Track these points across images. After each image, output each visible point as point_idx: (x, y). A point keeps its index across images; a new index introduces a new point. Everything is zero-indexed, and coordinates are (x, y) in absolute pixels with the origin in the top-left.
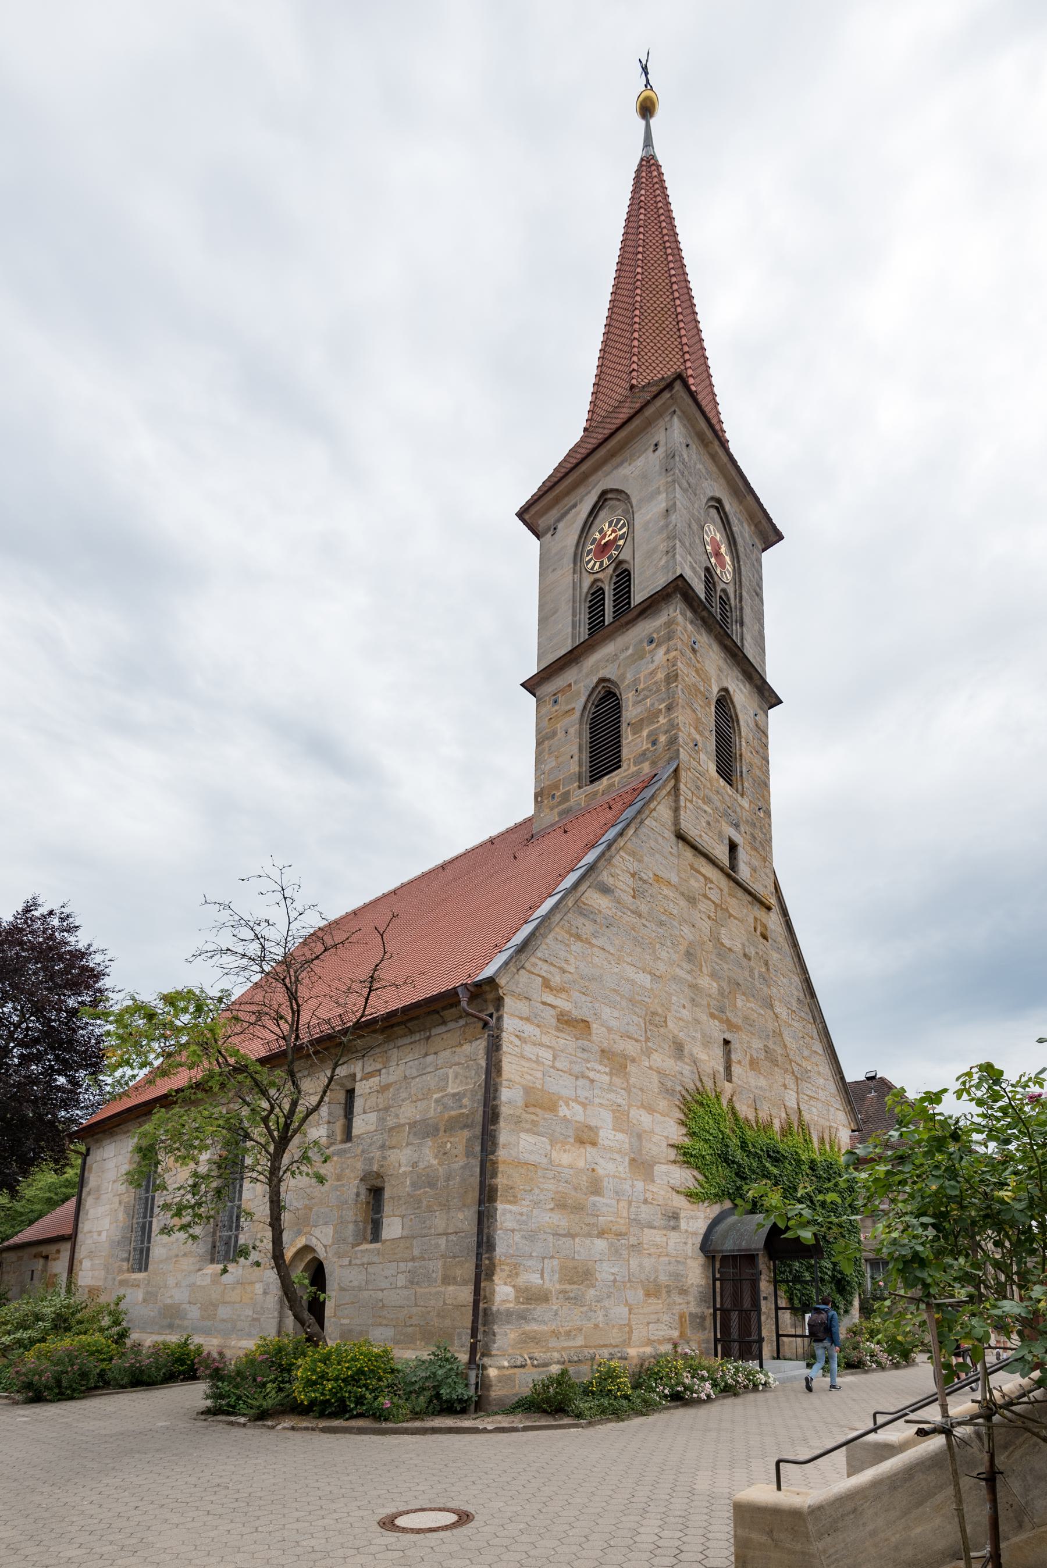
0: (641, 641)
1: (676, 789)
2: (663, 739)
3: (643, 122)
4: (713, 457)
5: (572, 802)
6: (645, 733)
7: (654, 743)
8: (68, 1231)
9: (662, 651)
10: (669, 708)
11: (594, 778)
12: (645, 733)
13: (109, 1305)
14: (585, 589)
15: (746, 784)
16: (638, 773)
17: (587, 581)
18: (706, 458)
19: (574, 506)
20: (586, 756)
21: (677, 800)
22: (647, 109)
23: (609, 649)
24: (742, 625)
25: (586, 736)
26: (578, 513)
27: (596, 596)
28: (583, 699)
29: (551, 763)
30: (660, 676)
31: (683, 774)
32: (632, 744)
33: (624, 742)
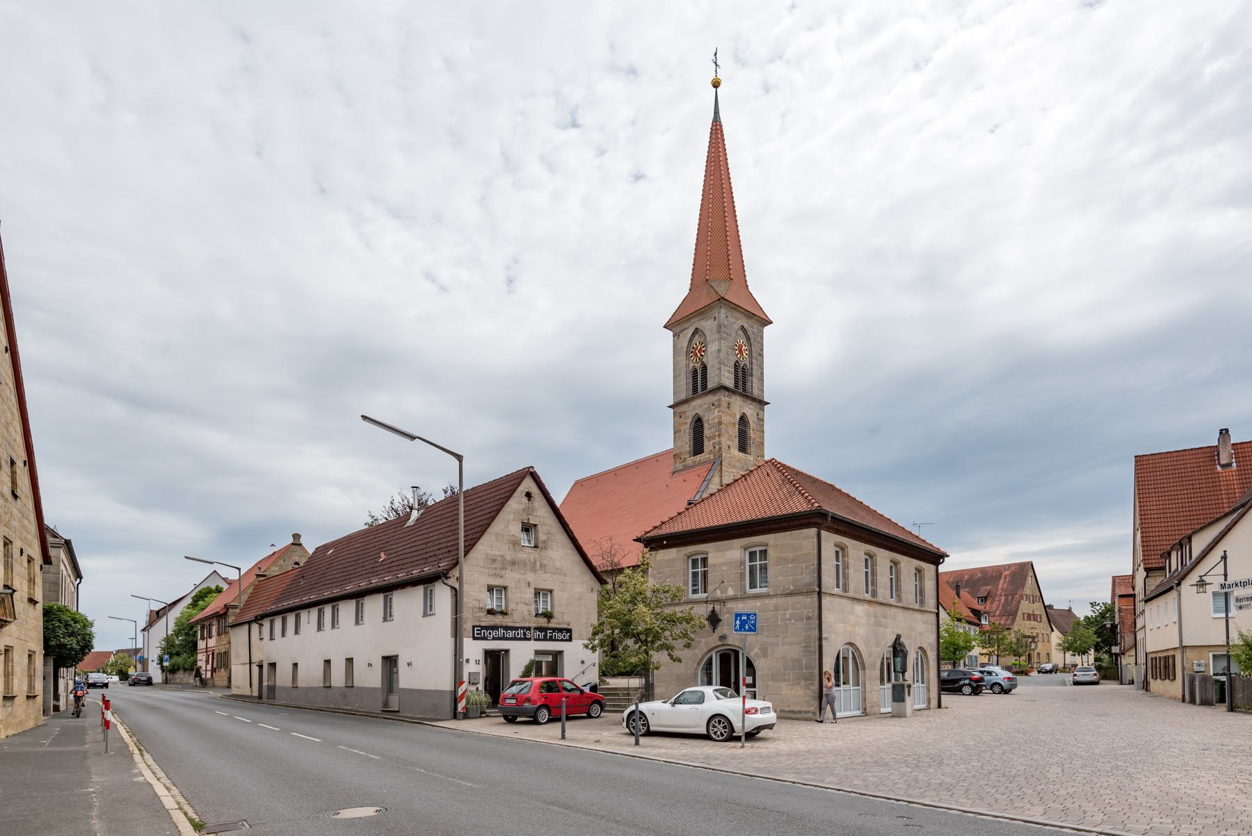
0: (710, 404)
1: (721, 469)
2: (717, 447)
3: (719, 76)
4: (739, 311)
5: (687, 462)
6: (711, 442)
7: (714, 448)
8: (1123, 682)
9: (717, 410)
10: (719, 435)
11: (695, 454)
12: (711, 442)
13: (605, 652)
14: (691, 369)
15: (752, 449)
16: (709, 458)
17: (691, 365)
18: (738, 313)
19: (686, 329)
20: (692, 443)
21: (721, 473)
22: (716, 85)
23: (699, 402)
24: (752, 376)
25: (692, 434)
26: (687, 333)
27: (695, 371)
28: (691, 420)
29: (679, 444)
30: (716, 421)
31: (723, 462)
32: (708, 445)
33: (705, 444)
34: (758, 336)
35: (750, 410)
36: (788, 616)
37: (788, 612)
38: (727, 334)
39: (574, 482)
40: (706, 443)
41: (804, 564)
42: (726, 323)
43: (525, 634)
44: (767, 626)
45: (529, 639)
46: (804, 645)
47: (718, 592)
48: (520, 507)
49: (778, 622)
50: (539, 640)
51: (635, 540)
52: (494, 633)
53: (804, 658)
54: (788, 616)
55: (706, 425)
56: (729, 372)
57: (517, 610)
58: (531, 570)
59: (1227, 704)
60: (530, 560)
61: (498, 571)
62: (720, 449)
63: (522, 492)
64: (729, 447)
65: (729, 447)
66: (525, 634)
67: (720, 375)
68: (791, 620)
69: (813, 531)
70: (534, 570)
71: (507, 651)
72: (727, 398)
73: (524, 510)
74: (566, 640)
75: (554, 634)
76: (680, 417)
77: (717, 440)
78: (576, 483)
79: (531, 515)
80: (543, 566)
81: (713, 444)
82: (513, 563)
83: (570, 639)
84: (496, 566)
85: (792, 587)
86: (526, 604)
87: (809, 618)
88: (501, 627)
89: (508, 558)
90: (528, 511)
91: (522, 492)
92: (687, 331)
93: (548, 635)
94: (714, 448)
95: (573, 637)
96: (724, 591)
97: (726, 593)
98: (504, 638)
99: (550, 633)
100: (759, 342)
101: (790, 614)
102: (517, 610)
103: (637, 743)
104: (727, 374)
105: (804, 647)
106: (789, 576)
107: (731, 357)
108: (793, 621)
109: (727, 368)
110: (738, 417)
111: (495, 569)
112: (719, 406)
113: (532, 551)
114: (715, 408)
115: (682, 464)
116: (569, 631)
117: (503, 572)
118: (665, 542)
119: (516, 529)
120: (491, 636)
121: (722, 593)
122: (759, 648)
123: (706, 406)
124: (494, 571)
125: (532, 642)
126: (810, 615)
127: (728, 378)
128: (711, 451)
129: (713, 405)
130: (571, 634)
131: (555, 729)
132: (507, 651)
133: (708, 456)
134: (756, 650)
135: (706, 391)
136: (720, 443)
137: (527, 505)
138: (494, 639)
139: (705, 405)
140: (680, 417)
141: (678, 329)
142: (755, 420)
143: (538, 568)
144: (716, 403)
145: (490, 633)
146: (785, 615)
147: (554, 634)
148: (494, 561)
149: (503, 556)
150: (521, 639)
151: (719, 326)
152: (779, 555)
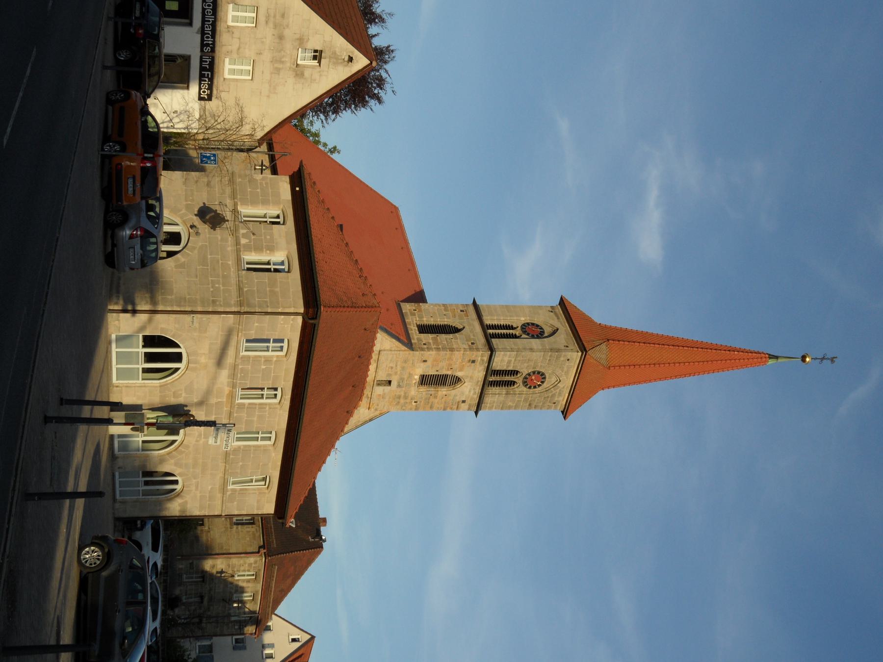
2: (425, 346)
7: (424, 344)
9: (466, 347)
16: (414, 339)
19: (558, 318)
30: (455, 346)
32: (428, 338)
33: (430, 335)
34: (550, 402)
35: (469, 390)
36: (217, 285)
37: (221, 286)
38: (550, 360)
39: (397, 206)
40: (430, 336)
41: (268, 300)
42: (562, 359)
43: (208, 45)
44: (208, 269)
45: (202, 50)
46: (188, 297)
47: (245, 231)
48: (337, 50)
49: (211, 278)
50: (201, 61)
51: (301, 162)
52: (209, 10)
53: (173, 297)
54: (217, 285)
55: (451, 336)
56: (509, 362)
57: (232, 38)
58: (273, 58)
59: (163, 54)
60: (284, 56)
61: (272, 19)
62: (422, 350)
63: (353, 52)
64: (425, 361)
65: (425, 361)
66: (208, 45)
67: (505, 350)
68: (212, 287)
69: (302, 310)
70: (274, 61)
71: (190, 24)
72: (479, 359)
73: (334, 53)
74: (200, 94)
75: (207, 79)
76: (461, 311)
77: (433, 347)
78: (396, 208)
79: (330, 61)
80: (278, 71)
81: (429, 343)
82: (281, 37)
83: (201, 99)
84: (277, 18)
85: (245, 289)
86: (239, 49)
87: (214, 302)
88: (215, 18)
89: (287, 33)
90: (336, 59)
91: (353, 52)
92: (556, 320)
93: (206, 73)
94: (424, 344)
95: (203, 102)
96: (244, 236)
97: (243, 237)
98: (204, 21)
99: (208, 74)
100: (544, 403)
101: (219, 288)
102: (232, 38)
103: (105, 68)
104: (506, 359)
105: (185, 298)
106: (257, 287)
107: (526, 365)
108: (212, 289)
109: (513, 360)
110: (459, 374)
111: (275, 17)
112: (471, 349)
113: (293, 61)
114: (469, 346)
115: (408, 311)
116: (210, 98)
117: (271, 25)
118: (297, 189)
119: (315, 43)
120: (207, 7)
121: (243, 234)
122: (185, 261)
123: (472, 337)
124: (272, 15)
125: (199, 54)
126: (218, 303)
127: (502, 361)
128: (421, 340)
129: (473, 344)
130: (206, 100)
131: (110, 62)
132: (190, 24)
133: (415, 337)
134: (183, 260)
135: (488, 338)
136: (429, 349)
137: (340, 58)
138: (204, 10)
139: (474, 336)
140: (461, 311)
141: (559, 310)
142: (458, 399)
143: (276, 65)
144: (474, 346)
145: (209, 6)
146: (219, 283)
147: (207, 79)
148: (283, 16)
149: (288, 26)
150: (202, 40)
151: (558, 350)
152: (278, 280)
